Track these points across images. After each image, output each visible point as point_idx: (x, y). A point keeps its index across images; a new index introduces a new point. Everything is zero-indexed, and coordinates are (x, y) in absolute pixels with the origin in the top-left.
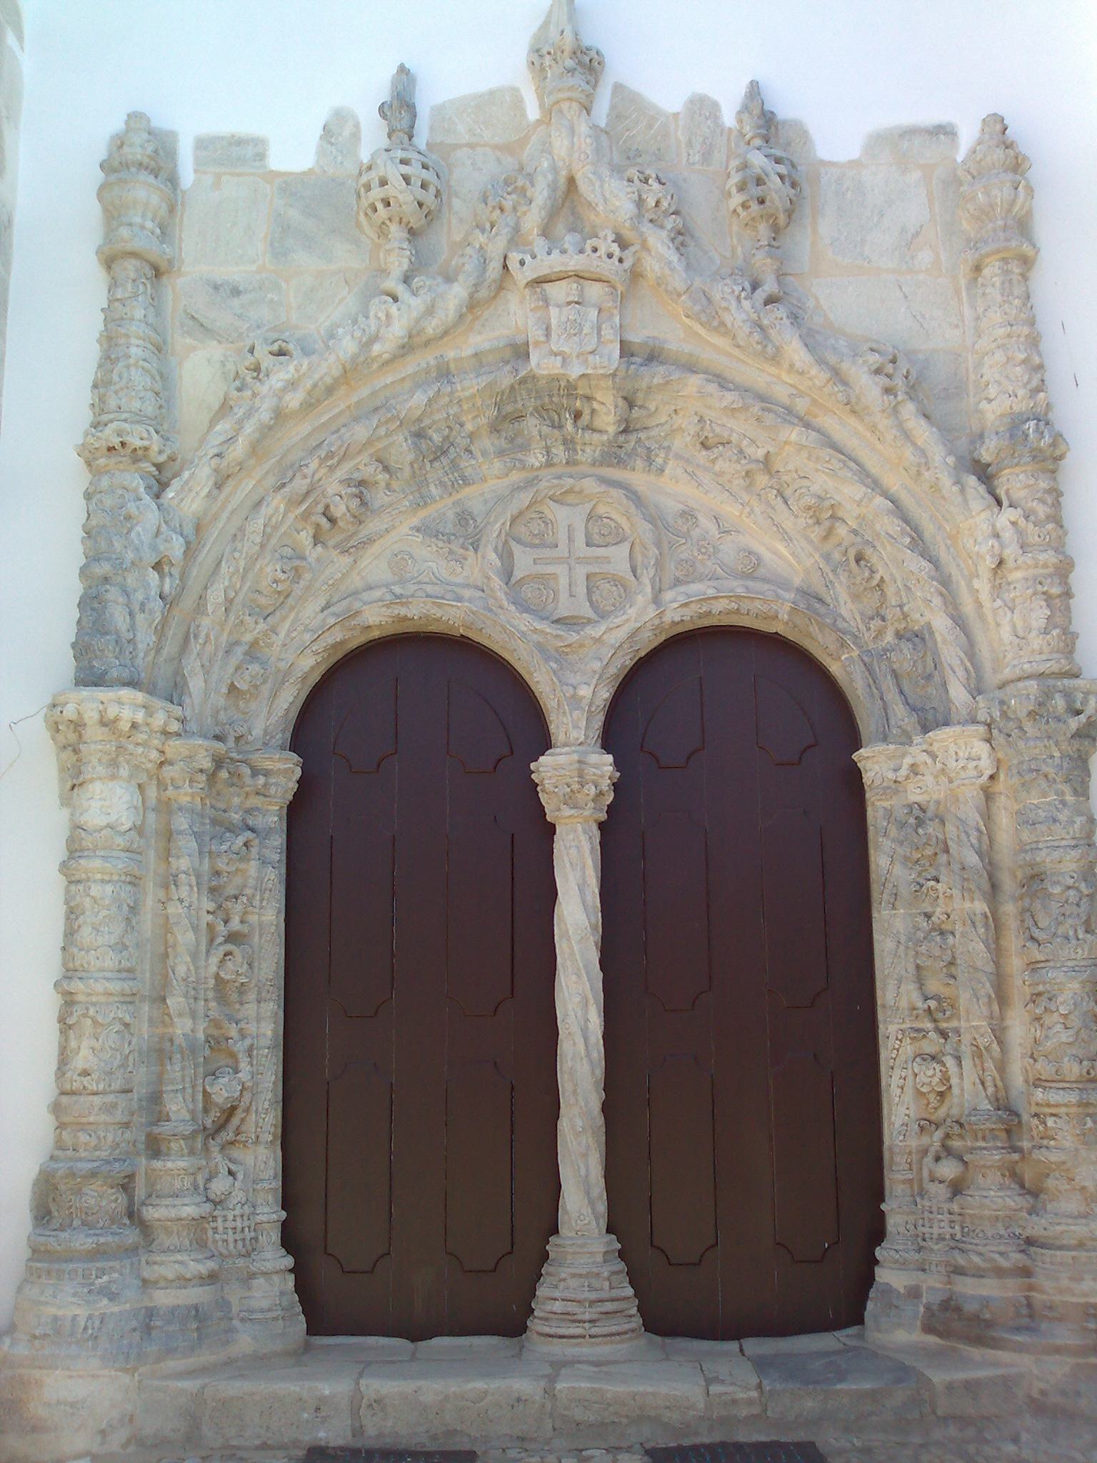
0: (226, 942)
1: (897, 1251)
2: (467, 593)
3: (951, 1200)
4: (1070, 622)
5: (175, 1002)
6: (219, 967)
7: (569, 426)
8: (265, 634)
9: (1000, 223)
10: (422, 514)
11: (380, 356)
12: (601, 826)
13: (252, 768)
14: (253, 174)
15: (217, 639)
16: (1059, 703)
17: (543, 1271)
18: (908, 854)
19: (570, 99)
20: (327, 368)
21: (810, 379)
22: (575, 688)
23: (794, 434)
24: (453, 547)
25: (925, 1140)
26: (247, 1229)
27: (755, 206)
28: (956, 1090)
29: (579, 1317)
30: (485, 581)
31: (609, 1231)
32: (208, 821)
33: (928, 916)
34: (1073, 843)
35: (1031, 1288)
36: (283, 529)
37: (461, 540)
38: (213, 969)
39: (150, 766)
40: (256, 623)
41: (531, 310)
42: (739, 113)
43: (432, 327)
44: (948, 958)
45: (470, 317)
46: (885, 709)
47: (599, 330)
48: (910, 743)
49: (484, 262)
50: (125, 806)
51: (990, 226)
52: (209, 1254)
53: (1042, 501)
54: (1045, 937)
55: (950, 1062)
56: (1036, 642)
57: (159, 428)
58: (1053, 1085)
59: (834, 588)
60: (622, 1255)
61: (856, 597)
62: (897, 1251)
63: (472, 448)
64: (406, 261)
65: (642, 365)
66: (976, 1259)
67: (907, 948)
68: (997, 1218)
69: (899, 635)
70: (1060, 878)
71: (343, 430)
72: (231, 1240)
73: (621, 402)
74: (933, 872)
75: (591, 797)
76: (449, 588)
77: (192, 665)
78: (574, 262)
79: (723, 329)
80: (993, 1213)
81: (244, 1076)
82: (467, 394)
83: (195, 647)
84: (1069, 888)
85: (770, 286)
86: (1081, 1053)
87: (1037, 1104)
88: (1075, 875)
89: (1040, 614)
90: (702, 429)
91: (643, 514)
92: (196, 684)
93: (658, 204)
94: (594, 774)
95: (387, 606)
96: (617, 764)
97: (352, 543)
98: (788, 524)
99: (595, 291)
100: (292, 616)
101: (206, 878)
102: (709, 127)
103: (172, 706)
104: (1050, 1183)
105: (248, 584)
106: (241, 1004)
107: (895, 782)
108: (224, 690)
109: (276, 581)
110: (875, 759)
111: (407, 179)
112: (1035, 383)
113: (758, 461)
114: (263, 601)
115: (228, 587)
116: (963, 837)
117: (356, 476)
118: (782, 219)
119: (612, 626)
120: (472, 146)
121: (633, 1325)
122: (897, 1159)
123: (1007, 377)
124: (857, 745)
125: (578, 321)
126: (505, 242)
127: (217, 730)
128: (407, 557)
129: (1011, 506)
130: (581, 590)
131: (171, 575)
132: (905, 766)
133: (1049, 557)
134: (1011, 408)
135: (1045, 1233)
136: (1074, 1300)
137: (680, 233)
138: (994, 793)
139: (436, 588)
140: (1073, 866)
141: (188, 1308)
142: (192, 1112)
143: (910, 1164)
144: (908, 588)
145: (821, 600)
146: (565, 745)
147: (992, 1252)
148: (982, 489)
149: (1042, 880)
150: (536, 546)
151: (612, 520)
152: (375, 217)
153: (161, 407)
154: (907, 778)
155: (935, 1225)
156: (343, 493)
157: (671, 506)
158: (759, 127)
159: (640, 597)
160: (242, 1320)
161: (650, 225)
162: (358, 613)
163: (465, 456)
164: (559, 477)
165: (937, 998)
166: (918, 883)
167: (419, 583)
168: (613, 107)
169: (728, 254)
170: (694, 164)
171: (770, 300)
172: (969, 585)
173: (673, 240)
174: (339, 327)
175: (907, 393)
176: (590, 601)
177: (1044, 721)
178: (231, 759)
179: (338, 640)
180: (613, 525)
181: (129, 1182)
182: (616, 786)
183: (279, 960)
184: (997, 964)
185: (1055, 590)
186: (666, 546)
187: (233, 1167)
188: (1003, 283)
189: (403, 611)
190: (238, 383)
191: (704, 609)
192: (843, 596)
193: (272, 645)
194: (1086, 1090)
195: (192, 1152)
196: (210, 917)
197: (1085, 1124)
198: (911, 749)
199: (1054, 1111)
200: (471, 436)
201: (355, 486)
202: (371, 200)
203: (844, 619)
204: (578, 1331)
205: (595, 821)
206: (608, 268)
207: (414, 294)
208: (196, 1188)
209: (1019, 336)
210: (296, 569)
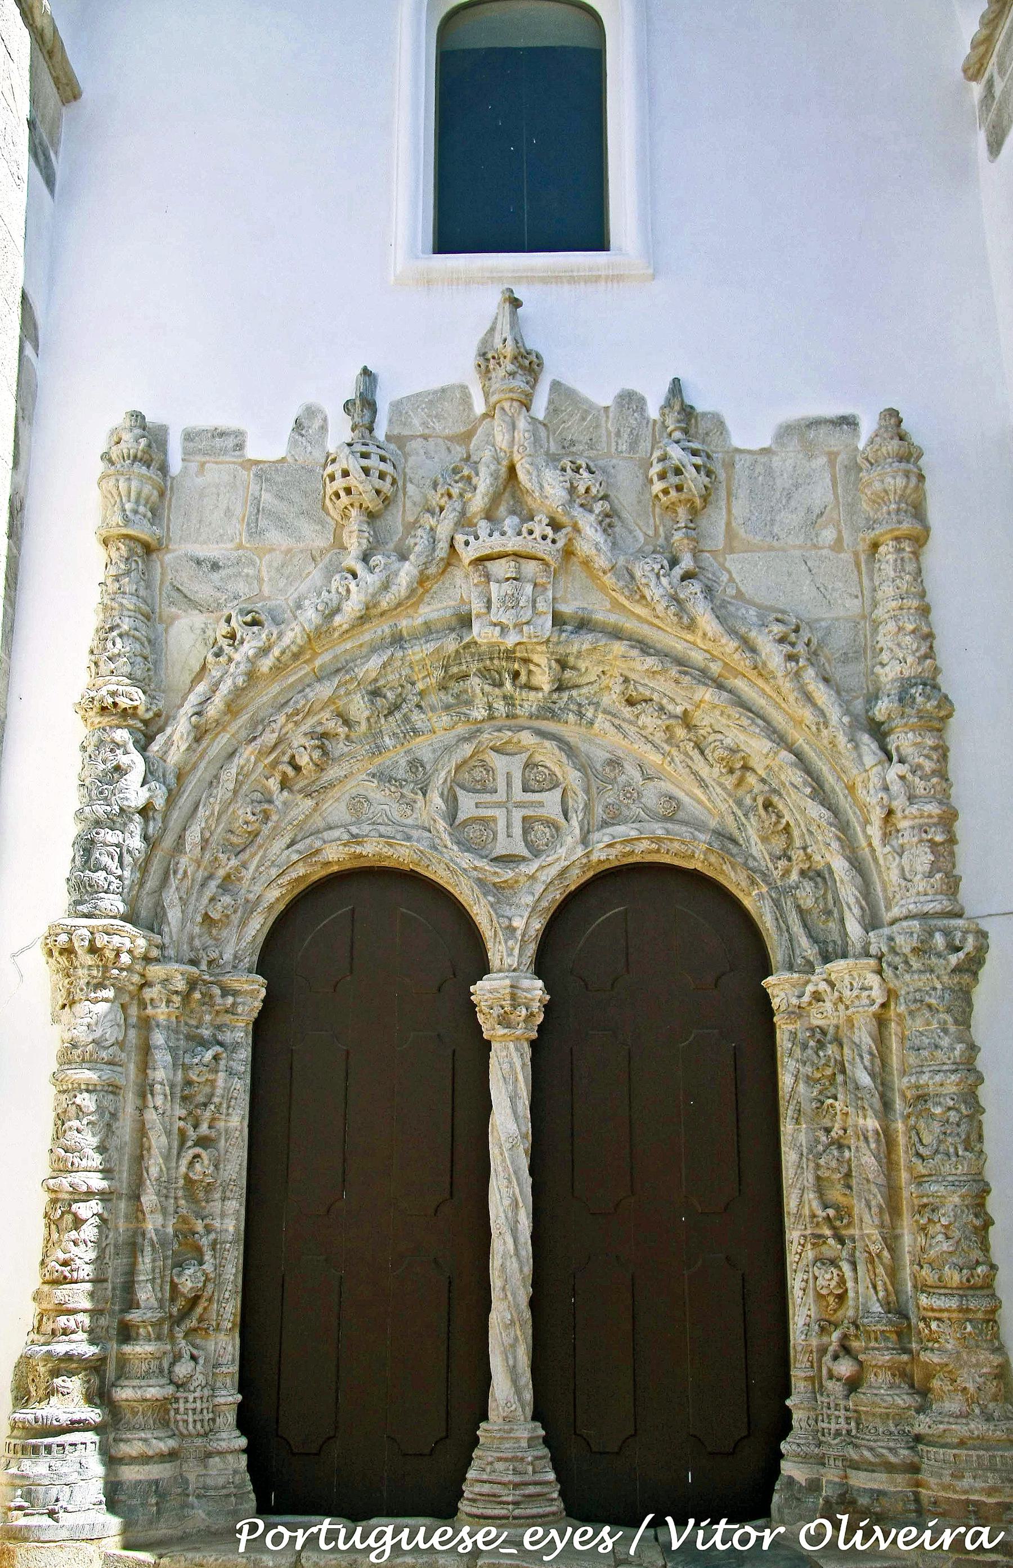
0: (195, 1145)
1: (798, 1445)
2: (415, 834)
3: (847, 1397)
4: (954, 866)
5: (149, 1199)
6: (188, 1168)
7: (508, 684)
8: (237, 869)
9: (893, 506)
10: (378, 760)
11: (340, 626)
12: (533, 1044)
13: (222, 989)
14: (234, 463)
15: (193, 875)
16: (939, 940)
17: (474, 1455)
18: (810, 1074)
19: (512, 400)
20: (292, 636)
21: (722, 646)
22: (510, 920)
23: (707, 694)
24: (404, 791)
25: (825, 1339)
26: (205, 1411)
27: (673, 493)
28: (851, 1294)
29: (504, 1499)
30: (432, 822)
31: (534, 1418)
32: (182, 1037)
33: (828, 1131)
34: (954, 1067)
35: (918, 1484)
36: (253, 777)
37: (412, 785)
38: (183, 1169)
39: (131, 988)
40: (229, 859)
41: (475, 585)
42: (663, 408)
43: (386, 601)
44: (844, 1170)
45: (421, 591)
46: (791, 940)
47: (534, 601)
48: (813, 972)
49: (434, 541)
50: (109, 1024)
51: (885, 508)
52: (170, 1433)
53: (927, 757)
54: (928, 1153)
55: (846, 1267)
56: (921, 884)
57: (147, 688)
58: (937, 1291)
59: (745, 831)
60: (546, 1441)
61: (765, 840)
62: (798, 1445)
63: (423, 704)
64: (365, 541)
65: (572, 633)
66: (867, 1454)
67: (808, 1159)
68: (888, 1415)
69: (803, 873)
70: (942, 1099)
71: (308, 690)
72: (191, 1420)
73: (553, 664)
74: (833, 1090)
75: (521, 1019)
76: (401, 829)
77: (171, 896)
78: (512, 543)
79: (644, 602)
80: (883, 1410)
81: (208, 1267)
82: (417, 658)
83: (174, 882)
84: (949, 1109)
85: (687, 563)
86: (961, 1262)
87: (924, 1309)
88: (955, 1097)
89: (924, 858)
90: (627, 688)
91: (573, 763)
92: (174, 915)
93: (588, 490)
94: (526, 998)
95: (345, 845)
96: (548, 988)
97: (314, 788)
98: (704, 772)
99: (530, 568)
100: (260, 854)
101: (179, 1088)
102: (636, 419)
103: (152, 934)
104: (936, 1384)
105: (222, 826)
106: (207, 1202)
107: (799, 1007)
108: (199, 919)
109: (247, 823)
110: (781, 987)
111: (366, 471)
112: (923, 650)
113: (677, 717)
114: (235, 840)
115: (203, 829)
116: (857, 1059)
117: (319, 729)
118: (698, 502)
119: (544, 864)
120: (426, 438)
121: (554, 1509)
122: (800, 1357)
123: (899, 645)
124: (768, 972)
125: (516, 595)
126: (452, 525)
127: (192, 955)
128: (363, 800)
129: (900, 761)
130: (517, 830)
131: (154, 819)
132: (807, 994)
133: (933, 809)
134: (901, 673)
135: (930, 1432)
136: (955, 1496)
137: (607, 516)
138: (887, 1020)
139: (389, 828)
140: (954, 1089)
141: (150, 1483)
142: (161, 1301)
143: (812, 1362)
144: (811, 833)
145: (734, 841)
146: (500, 971)
147: (882, 1447)
148: (874, 746)
149: (926, 1101)
150: (477, 791)
151: (546, 767)
152: (338, 502)
153: (149, 670)
154: (810, 1004)
155: (833, 1421)
156: (307, 745)
157: (600, 756)
158: (679, 421)
159: (569, 838)
160: (198, 1497)
161: (581, 510)
162: (318, 851)
163: (416, 711)
164: (499, 730)
165: (837, 1208)
166: (820, 1101)
167: (373, 823)
168: (551, 402)
169: (651, 533)
170: (622, 452)
171: (687, 576)
172: (864, 831)
173: (600, 523)
174: (306, 598)
175: (808, 659)
176: (525, 841)
177: (927, 956)
178: (203, 981)
179: (301, 874)
180: (546, 771)
181: (101, 1365)
182: (548, 1008)
183: (242, 1161)
184: (889, 1177)
185: (939, 838)
186: (594, 790)
187: (195, 1352)
188: (896, 560)
189: (359, 849)
190: (215, 649)
191: (628, 849)
192: (754, 838)
193: (242, 878)
194: (966, 1296)
195: (159, 1338)
196: (182, 1123)
197: (965, 1328)
198: (813, 978)
199: (937, 1315)
200: (421, 694)
201: (318, 739)
202: (335, 489)
203: (755, 859)
204: (504, 1512)
205: (527, 1039)
206: (543, 549)
207: (371, 571)
208: (161, 1371)
209: (909, 608)
210: (265, 811)
